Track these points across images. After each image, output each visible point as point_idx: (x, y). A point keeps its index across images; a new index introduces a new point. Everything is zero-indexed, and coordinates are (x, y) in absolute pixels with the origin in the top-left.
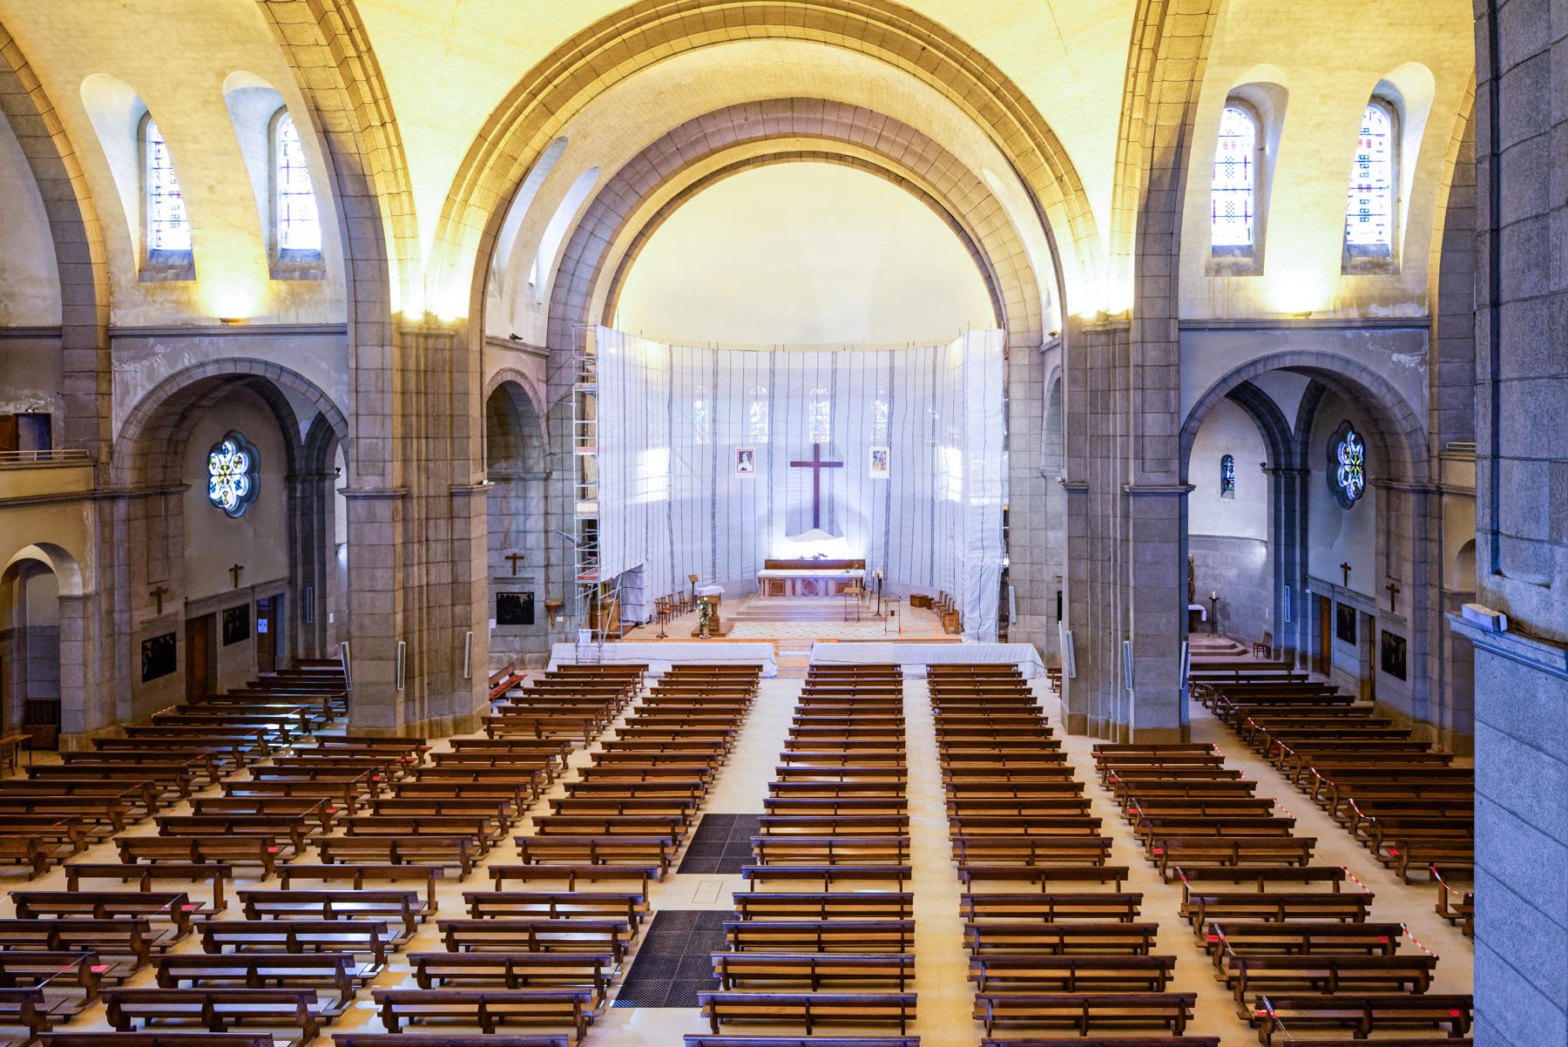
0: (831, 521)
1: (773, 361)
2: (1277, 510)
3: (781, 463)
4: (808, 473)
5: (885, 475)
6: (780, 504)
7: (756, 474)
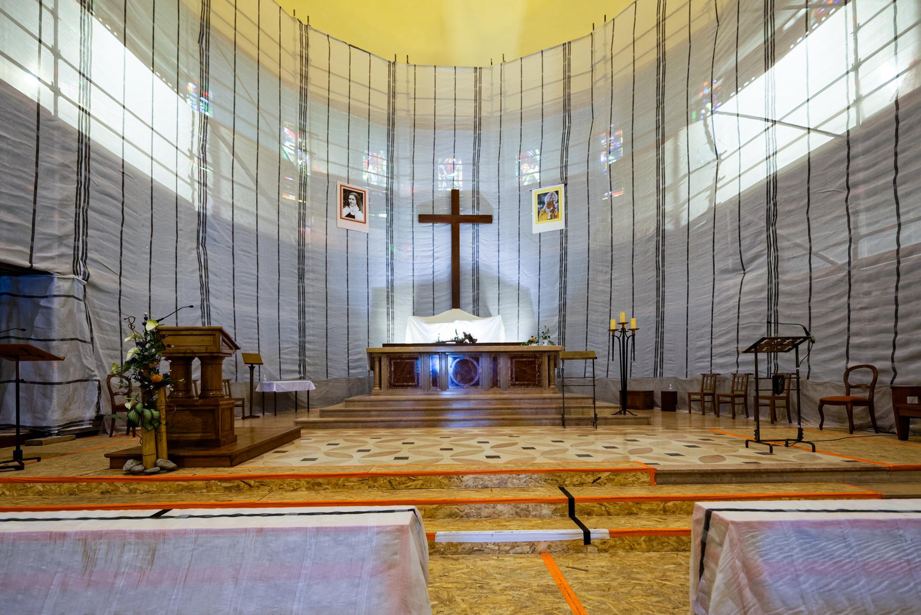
0: (476, 301)
1: (392, 75)
2: (756, 482)
3: (405, 217)
4: (443, 232)
5: (558, 224)
6: (403, 275)
7: (369, 228)
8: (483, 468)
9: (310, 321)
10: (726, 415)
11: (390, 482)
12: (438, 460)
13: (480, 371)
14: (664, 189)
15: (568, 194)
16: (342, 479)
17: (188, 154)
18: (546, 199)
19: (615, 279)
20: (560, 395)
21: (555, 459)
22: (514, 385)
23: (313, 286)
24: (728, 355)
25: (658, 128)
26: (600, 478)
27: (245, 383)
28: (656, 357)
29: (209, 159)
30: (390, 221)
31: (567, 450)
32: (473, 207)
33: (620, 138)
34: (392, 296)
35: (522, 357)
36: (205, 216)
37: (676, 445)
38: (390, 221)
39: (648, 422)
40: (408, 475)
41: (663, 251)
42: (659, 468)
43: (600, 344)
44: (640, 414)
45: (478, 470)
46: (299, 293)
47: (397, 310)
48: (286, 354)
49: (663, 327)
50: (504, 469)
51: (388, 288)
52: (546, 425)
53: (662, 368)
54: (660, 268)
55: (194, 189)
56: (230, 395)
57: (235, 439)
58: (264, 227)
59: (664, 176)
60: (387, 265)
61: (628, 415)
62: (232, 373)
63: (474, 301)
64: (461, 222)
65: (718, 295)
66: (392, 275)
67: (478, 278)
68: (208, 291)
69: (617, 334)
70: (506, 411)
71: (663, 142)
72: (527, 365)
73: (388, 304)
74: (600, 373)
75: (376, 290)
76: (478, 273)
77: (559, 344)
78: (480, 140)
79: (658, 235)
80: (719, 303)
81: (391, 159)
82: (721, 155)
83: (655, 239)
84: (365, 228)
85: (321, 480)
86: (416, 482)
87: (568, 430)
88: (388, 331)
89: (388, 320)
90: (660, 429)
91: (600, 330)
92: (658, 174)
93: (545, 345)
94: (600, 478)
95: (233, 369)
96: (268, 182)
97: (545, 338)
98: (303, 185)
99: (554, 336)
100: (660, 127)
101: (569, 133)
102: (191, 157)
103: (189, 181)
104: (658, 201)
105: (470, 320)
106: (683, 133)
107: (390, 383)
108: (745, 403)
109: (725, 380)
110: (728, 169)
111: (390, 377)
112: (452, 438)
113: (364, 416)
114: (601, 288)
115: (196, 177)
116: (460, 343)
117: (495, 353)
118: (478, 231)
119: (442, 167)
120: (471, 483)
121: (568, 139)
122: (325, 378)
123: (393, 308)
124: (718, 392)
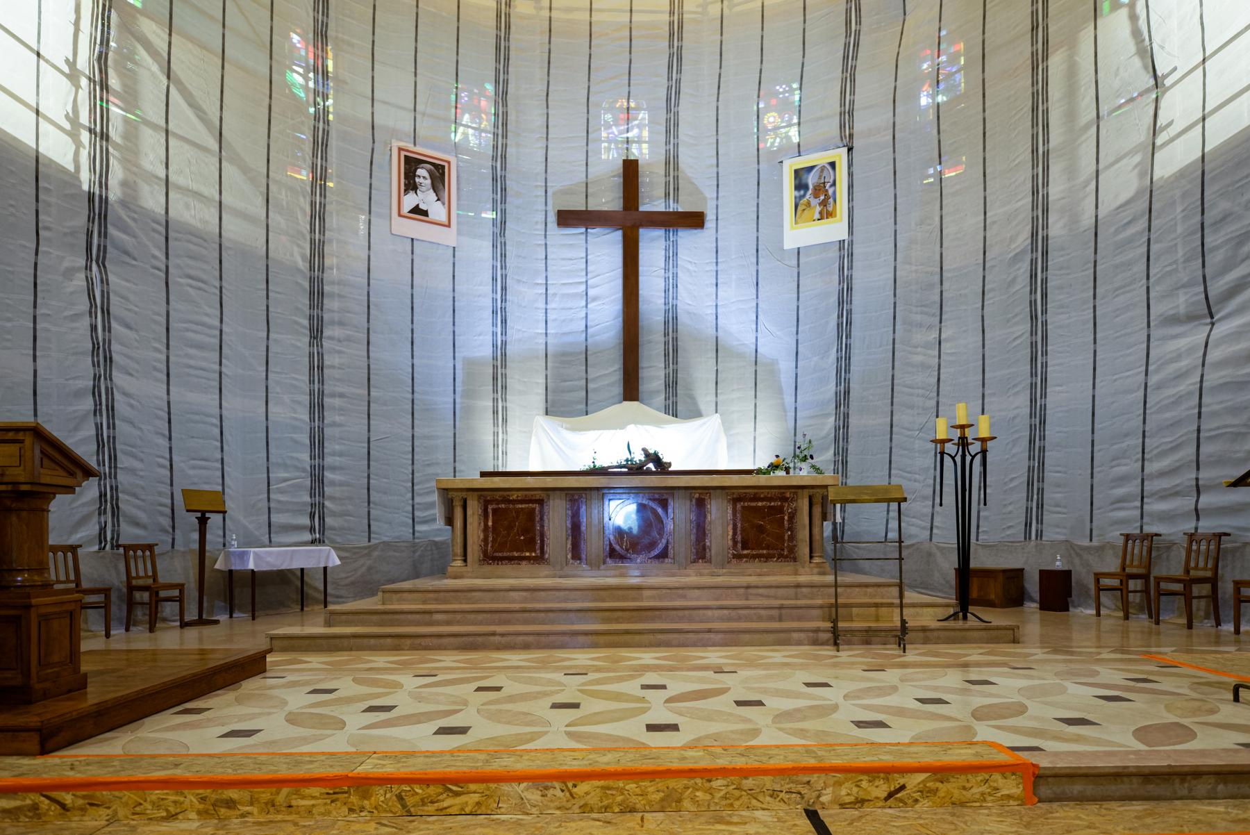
0: (672, 385)
4: (605, 248)
5: (835, 230)
6: (527, 330)
7: (454, 238)
8: (628, 762)
9: (334, 424)
10: (1173, 618)
11: (400, 798)
12: (533, 737)
13: (669, 526)
14: (1046, 154)
15: (855, 169)
16: (285, 791)
17: (66, 69)
18: (811, 180)
19: (947, 340)
20: (830, 579)
21: (802, 733)
22: (738, 557)
23: (340, 356)
24: (1177, 494)
25: (1034, 28)
26: (903, 787)
27: (191, 551)
28: (1029, 498)
29: (114, 81)
30: (501, 225)
31: (835, 708)
32: (667, 195)
33: (958, 51)
34: (504, 376)
35: (756, 498)
36: (104, 201)
37: (1078, 695)
38: (501, 225)
39: (1014, 637)
40: (444, 782)
41: (1045, 281)
42: (1044, 762)
43: (916, 471)
44: (998, 618)
45: (612, 767)
46: (311, 368)
47: (514, 403)
48: (281, 491)
49: (1043, 438)
50: (676, 765)
51: (495, 358)
52: (799, 643)
53: (1040, 521)
54: (1037, 316)
55: (78, 144)
56: (155, 577)
57: (81, 684)
58: (232, 228)
59: (1046, 126)
60: (494, 312)
61: (972, 622)
62: (164, 531)
63: (667, 386)
64: (642, 225)
65: (1157, 371)
66: (504, 333)
67: (675, 340)
68: (109, 360)
69: (951, 448)
70: (717, 613)
71: (1046, 57)
72: (765, 517)
73: (495, 391)
74: (915, 530)
75: (470, 363)
76: (675, 330)
77: (836, 471)
78: (680, 59)
79: (1034, 249)
80: (1159, 387)
81: (502, 95)
82: (1165, 76)
83: (1028, 258)
84: (448, 237)
85: (233, 794)
86: (463, 799)
87: (845, 655)
88: (495, 446)
89: (495, 424)
90: (1039, 653)
91: (917, 444)
92: (1034, 124)
93: (803, 474)
94: (903, 787)
95: (166, 522)
96: (244, 134)
97: (804, 459)
98: (321, 144)
99: (825, 458)
100: (1038, 26)
101: (857, 45)
102: (73, 76)
103: (67, 126)
104: (1034, 178)
105: (657, 423)
106: (1087, 35)
107: (485, 553)
108: (1214, 597)
109: (1170, 546)
110: (1179, 106)
111: (485, 540)
112: (592, 676)
113: (418, 624)
114: (919, 358)
115: (84, 118)
116: (635, 469)
117: (701, 491)
118: (675, 244)
119: (609, 117)
120: (593, 800)
121: (855, 58)
122: (364, 543)
123: (505, 400)
124: (1155, 572)
